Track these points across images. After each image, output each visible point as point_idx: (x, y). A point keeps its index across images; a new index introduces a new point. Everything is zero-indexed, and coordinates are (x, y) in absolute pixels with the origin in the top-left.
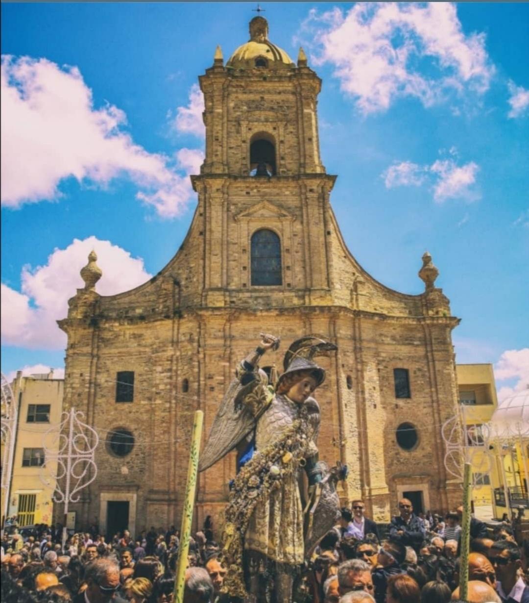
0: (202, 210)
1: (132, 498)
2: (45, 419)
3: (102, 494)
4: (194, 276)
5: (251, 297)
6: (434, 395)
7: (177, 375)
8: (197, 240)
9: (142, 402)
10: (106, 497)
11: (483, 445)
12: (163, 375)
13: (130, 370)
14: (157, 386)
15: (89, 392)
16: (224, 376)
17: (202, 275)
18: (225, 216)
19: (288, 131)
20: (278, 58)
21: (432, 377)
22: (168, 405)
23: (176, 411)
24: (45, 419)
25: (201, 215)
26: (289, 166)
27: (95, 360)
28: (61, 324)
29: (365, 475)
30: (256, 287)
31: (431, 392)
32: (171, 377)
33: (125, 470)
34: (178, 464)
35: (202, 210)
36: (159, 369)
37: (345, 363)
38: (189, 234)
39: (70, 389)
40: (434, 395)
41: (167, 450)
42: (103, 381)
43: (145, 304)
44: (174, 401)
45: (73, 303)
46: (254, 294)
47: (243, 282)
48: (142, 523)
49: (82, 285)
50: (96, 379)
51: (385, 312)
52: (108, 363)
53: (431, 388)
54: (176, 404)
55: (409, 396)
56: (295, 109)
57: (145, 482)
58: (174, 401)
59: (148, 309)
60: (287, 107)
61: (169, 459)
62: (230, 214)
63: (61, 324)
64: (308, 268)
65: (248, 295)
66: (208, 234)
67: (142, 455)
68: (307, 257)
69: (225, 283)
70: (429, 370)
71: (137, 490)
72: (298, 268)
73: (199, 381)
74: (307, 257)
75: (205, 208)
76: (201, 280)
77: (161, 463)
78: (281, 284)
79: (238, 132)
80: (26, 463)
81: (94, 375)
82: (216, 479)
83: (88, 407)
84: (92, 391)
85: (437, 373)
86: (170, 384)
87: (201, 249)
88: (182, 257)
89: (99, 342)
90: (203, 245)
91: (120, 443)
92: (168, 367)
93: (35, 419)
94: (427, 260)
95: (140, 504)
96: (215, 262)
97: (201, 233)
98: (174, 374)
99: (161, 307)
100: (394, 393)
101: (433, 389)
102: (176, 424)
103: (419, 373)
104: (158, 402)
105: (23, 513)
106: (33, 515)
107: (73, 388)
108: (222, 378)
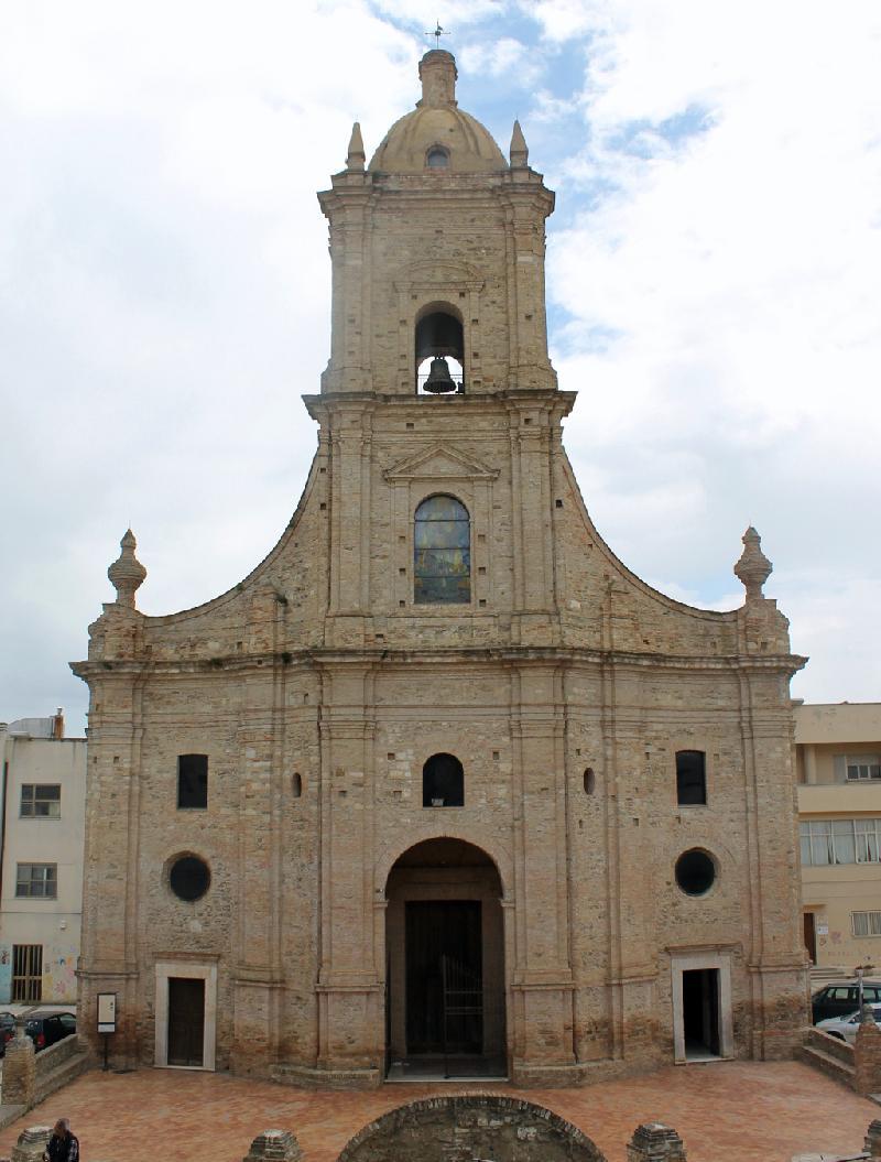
0: (324, 462)
1: (209, 974)
2: (50, 891)
3: (158, 966)
4: (310, 587)
5: (413, 627)
6: (751, 797)
7: (282, 766)
8: (315, 517)
9: (223, 811)
10: (165, 971)
11: (806, 907)
12: (257, 764)
13: (200, 752)
14: (247, 783)
15: (130, 790)
16: (364, 770)
17: (325, 587)
18: (367, 472)
19: (487, 299)
20: (472, 147)
21: (749, 765)
22: (267, 818)
23: (280, 829)
24: (50, 891)
25: (323, 470)
26: (487, 372)
27: (139, 733)
28: (78, 669)
29: (613, 942)
30: (424, 607)
31: (746, 793)
32: (271, 770)
33: (196, 926)
34: (286, 918)
35: (324, 462)
36: (251, 753)
37: (582, 747)
38: (301, 507)
39: (98, 785)
40: (751, 797)
41: (267, 897)
42: (153, 771)
43: (224, 633)
44: (277, 812)
45: (97, 631)
46: (419, 622)
47: (400, 597)
48: (227, 1015)
49: (111, 594)
50: (141, 766)
51: (664, 649)
52: (162, 737)
53: (746, 785)
54: (281, 816)
55: (703, 801)
56: (501, 254)
57: (229, 948)
58: (277, 812)
59: (231, 642)
60: (488, 249)
61: (271, 912)
62: (376, 467)
63: (78, 669)
64: (518, 571)
65: (409, 622)
66: (335, 506)
67: (226, 903)
68: (517, 551)
69: (366, 600)
70: (743, 753)
71: (217, 962)
72: (500, 572)
73: (320, 780)
74: (517, 551)
75: (330, 456)
76: (323, 596)
77: (256, 918)
78: (468, 601)
79: (393, 305)
80: (21, 891)
81: (138, 759)
82: (350, 950)
83: (129, 816)
84: (136, 789)
85: (757, 760)
86: (271, 781)
87: (324, 535)
88: (290, 547)
89: (143, 700)
90: (326, 528)
91: (189, 877)
92: (267, 752)
93: (34, 810)
94: (751, 539)
95: (223, 984)
96: (348, 561)
97: (323, 506)
98: (277, 763)
99: (253, 640)
100: (675, 797)
101: (749, 789)
102: (283, 850)
103: (723, 758)
104: (250, 812)
105: (22, 978)
106: (40, 982)
107: (102, 784)
108: (362, 774)
